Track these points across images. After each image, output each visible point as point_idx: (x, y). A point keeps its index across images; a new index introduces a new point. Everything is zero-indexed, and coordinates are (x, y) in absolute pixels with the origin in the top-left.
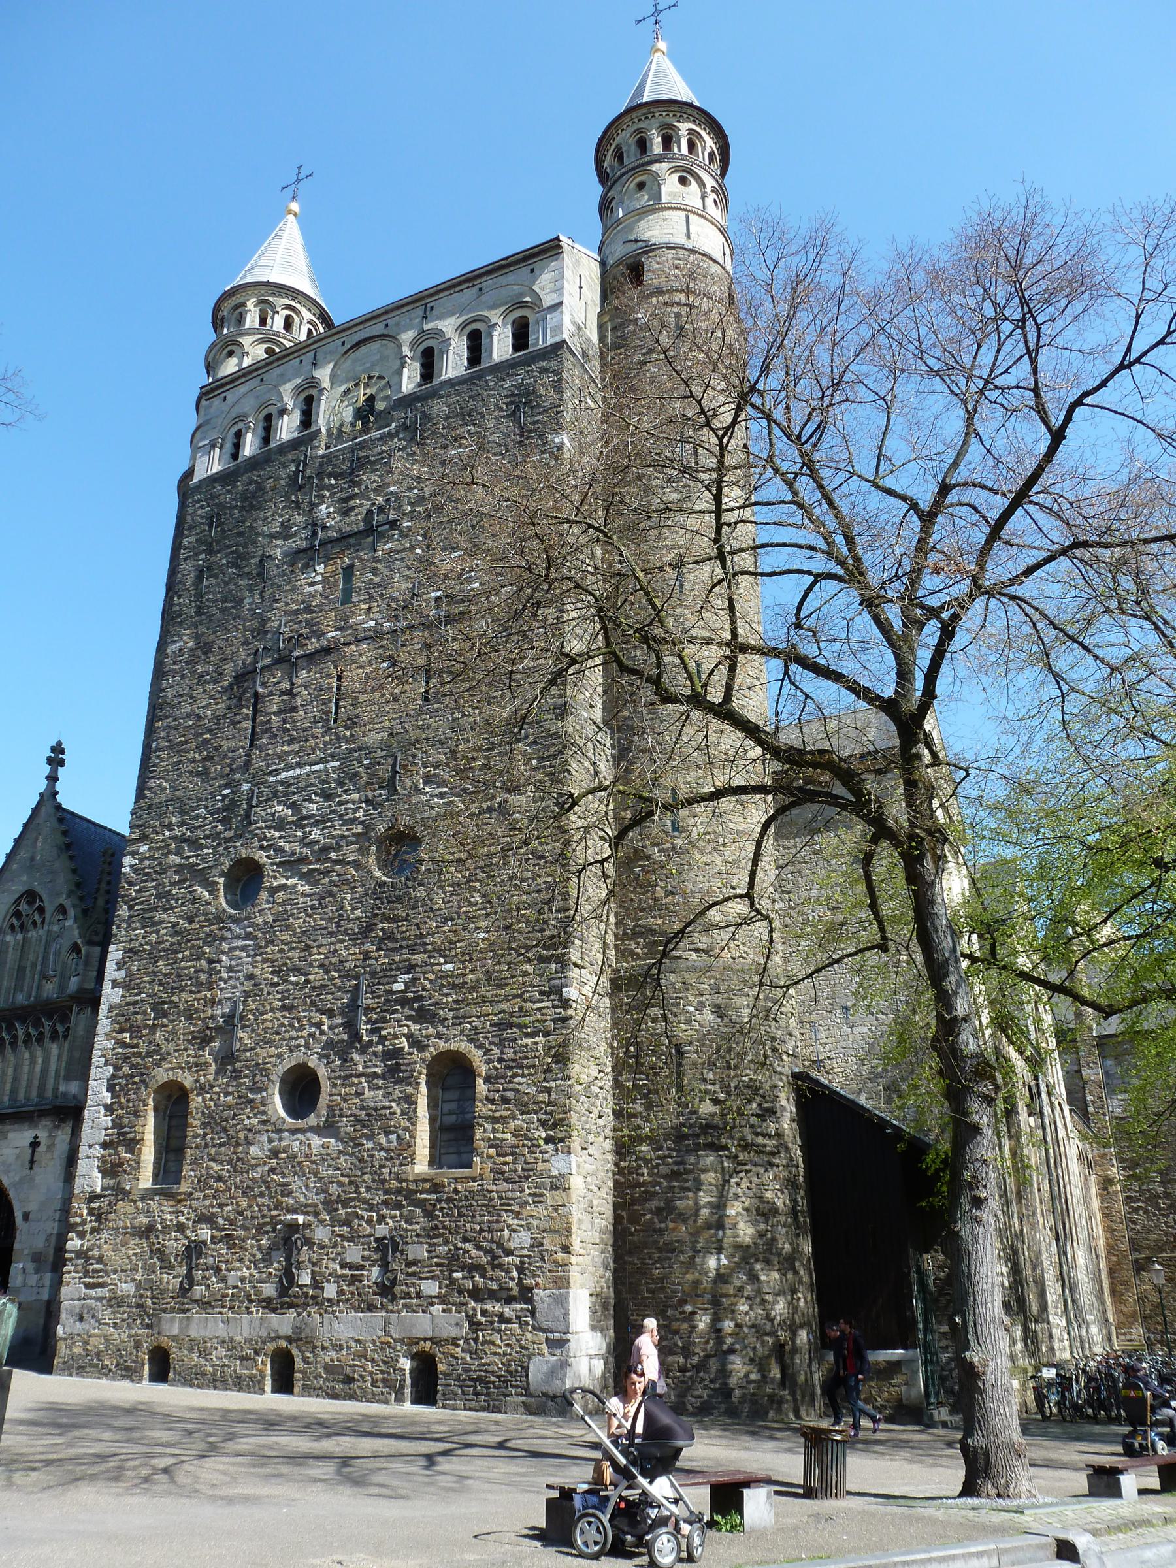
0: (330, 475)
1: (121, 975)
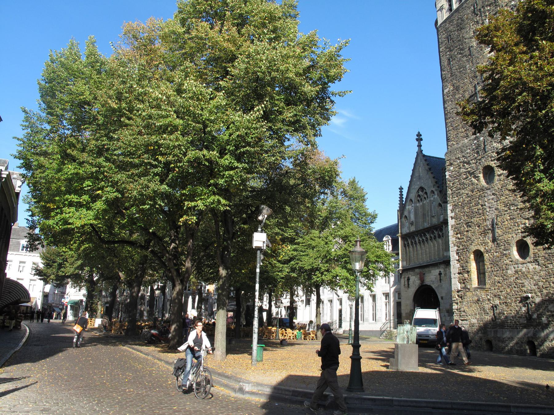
0: (487, 6)
1: (453, 215)
